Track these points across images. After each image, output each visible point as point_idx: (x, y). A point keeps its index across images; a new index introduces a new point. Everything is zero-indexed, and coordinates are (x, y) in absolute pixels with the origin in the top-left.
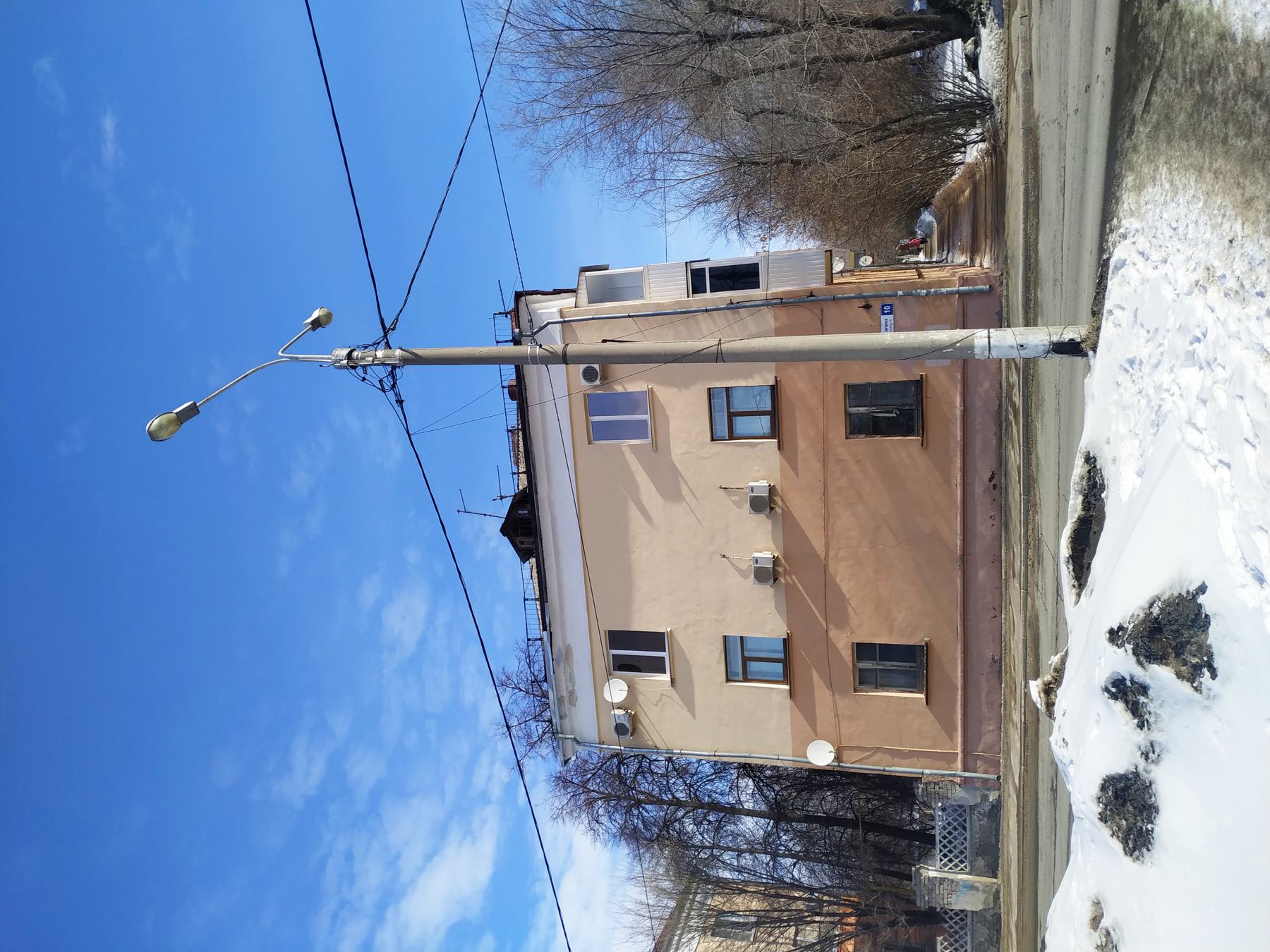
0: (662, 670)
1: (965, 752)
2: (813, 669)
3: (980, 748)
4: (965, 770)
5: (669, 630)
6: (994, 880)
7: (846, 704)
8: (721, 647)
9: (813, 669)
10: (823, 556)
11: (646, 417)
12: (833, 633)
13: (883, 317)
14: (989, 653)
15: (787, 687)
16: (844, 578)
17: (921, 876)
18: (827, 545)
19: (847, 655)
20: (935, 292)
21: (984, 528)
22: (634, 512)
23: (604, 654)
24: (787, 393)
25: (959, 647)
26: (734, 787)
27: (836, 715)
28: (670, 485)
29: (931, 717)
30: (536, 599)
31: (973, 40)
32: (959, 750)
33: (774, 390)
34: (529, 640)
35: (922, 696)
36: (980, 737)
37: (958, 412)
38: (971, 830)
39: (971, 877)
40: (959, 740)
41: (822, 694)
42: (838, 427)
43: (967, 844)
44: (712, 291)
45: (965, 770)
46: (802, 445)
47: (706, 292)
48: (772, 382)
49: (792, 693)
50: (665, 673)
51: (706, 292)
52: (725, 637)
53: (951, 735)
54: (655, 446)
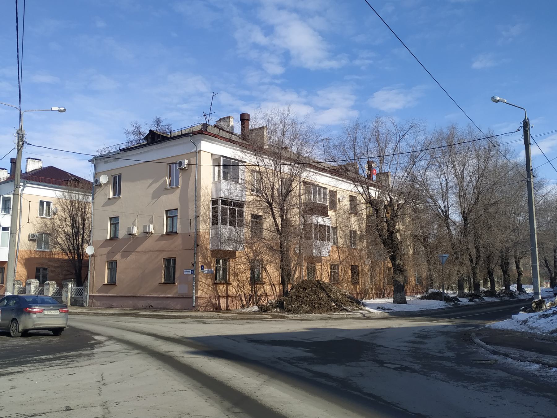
0: (114, 194)
1: (94, 296)
2: (111, 247)
3: (95, 301)
4: (90, 296)
5: (121, 197)
6: (69, 304)
7: (105, 258)
8: (117, 216)
9: (111, 247)
10: (136, 251)
11: (174, 186)
12: (119, 254)
13: (190, 270)
14: (114, 304)
15: (164, 233)
16: (132, 257)
17: (69, 282)
18: (139, 252)
19: (114, 259)
20: (193, 288)
21: (141, 303)
22: (150, 181)
23: (116, 173)
24: (175, 237)
25: (115, 295)
26: (473, 181)
27: (102, 255)
28: (156, 195)
29: (101, 286)
30: (109, 151)
31: (550, 303)
32: (94, 294)
33: (176, 233)
34: (119, 145)
35: (106, 282)
36: (97, 301)
37: (167, 296)
38: (80, 298)
39: (70, 297)
40: (96, 294)
41: (106, 250)
42: (167, 256)
43: (77, 296)
44: (213, 208)
45: (90, 296)
46: (163, 243)
47: (212, 205)
48: (178, 232)
49: (163, 235)
50: (113, 196)
51: (212, 205)
52: (119, 217)
53: (99, 291)
54: (166, 189)
